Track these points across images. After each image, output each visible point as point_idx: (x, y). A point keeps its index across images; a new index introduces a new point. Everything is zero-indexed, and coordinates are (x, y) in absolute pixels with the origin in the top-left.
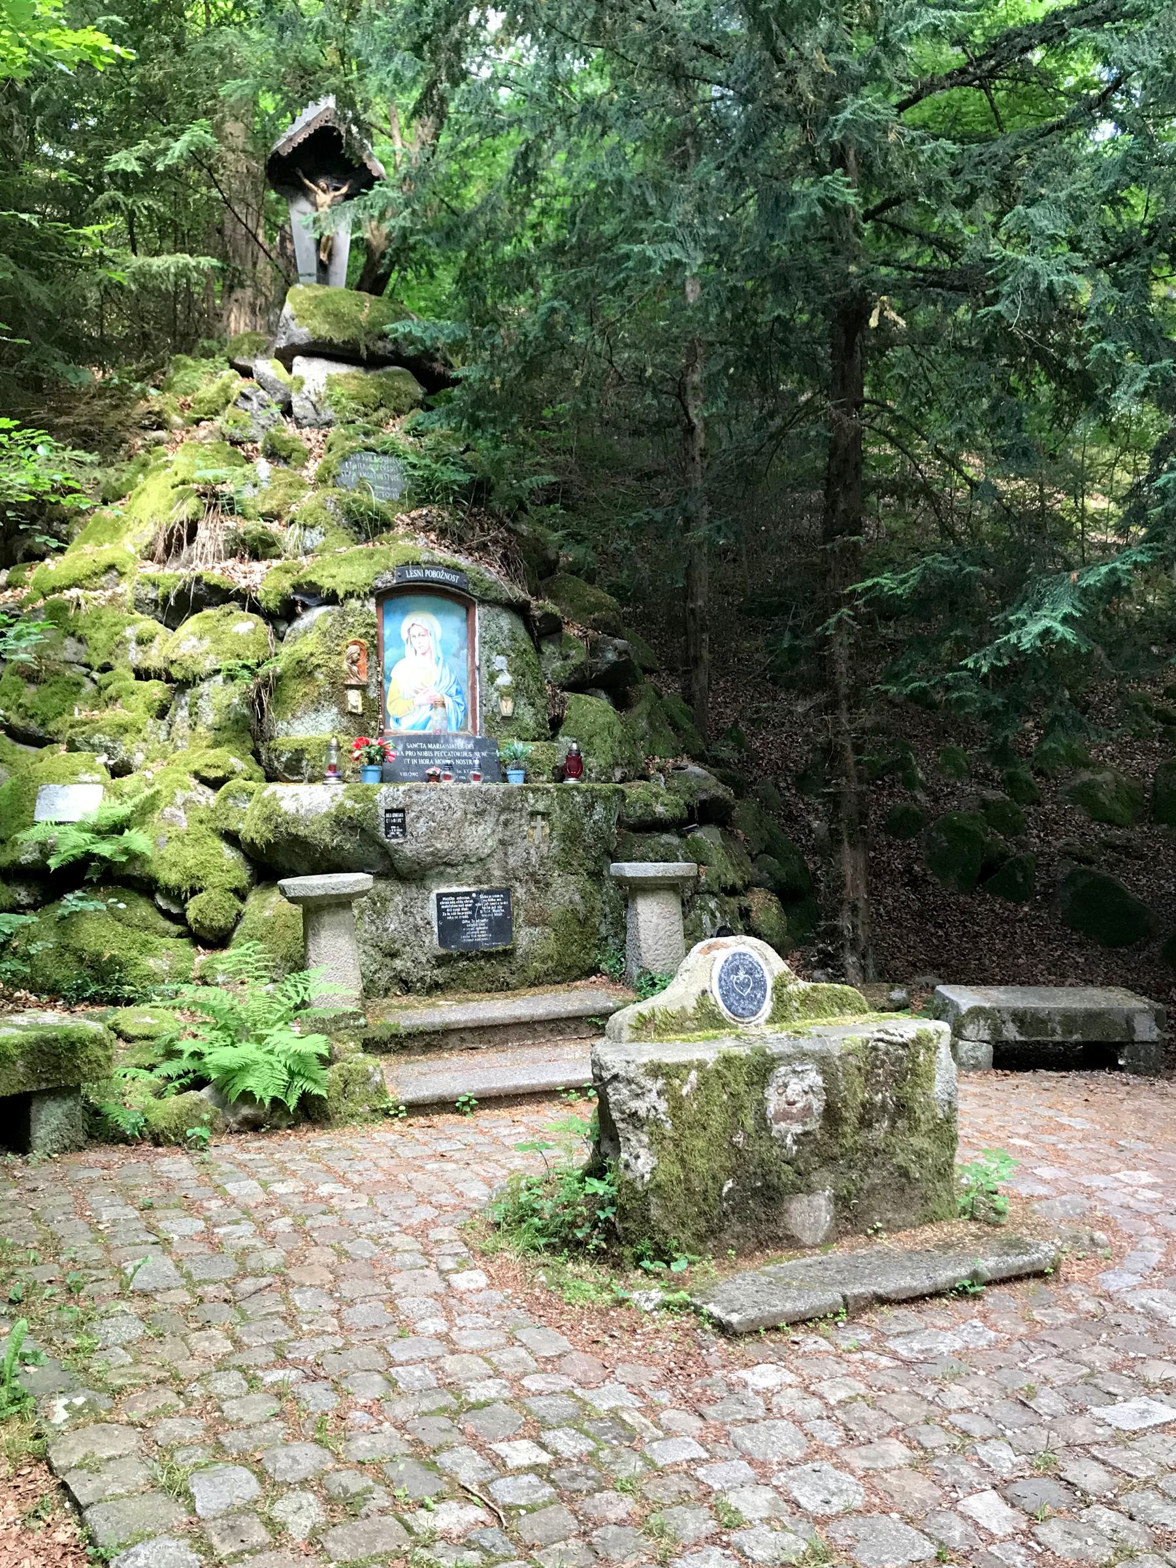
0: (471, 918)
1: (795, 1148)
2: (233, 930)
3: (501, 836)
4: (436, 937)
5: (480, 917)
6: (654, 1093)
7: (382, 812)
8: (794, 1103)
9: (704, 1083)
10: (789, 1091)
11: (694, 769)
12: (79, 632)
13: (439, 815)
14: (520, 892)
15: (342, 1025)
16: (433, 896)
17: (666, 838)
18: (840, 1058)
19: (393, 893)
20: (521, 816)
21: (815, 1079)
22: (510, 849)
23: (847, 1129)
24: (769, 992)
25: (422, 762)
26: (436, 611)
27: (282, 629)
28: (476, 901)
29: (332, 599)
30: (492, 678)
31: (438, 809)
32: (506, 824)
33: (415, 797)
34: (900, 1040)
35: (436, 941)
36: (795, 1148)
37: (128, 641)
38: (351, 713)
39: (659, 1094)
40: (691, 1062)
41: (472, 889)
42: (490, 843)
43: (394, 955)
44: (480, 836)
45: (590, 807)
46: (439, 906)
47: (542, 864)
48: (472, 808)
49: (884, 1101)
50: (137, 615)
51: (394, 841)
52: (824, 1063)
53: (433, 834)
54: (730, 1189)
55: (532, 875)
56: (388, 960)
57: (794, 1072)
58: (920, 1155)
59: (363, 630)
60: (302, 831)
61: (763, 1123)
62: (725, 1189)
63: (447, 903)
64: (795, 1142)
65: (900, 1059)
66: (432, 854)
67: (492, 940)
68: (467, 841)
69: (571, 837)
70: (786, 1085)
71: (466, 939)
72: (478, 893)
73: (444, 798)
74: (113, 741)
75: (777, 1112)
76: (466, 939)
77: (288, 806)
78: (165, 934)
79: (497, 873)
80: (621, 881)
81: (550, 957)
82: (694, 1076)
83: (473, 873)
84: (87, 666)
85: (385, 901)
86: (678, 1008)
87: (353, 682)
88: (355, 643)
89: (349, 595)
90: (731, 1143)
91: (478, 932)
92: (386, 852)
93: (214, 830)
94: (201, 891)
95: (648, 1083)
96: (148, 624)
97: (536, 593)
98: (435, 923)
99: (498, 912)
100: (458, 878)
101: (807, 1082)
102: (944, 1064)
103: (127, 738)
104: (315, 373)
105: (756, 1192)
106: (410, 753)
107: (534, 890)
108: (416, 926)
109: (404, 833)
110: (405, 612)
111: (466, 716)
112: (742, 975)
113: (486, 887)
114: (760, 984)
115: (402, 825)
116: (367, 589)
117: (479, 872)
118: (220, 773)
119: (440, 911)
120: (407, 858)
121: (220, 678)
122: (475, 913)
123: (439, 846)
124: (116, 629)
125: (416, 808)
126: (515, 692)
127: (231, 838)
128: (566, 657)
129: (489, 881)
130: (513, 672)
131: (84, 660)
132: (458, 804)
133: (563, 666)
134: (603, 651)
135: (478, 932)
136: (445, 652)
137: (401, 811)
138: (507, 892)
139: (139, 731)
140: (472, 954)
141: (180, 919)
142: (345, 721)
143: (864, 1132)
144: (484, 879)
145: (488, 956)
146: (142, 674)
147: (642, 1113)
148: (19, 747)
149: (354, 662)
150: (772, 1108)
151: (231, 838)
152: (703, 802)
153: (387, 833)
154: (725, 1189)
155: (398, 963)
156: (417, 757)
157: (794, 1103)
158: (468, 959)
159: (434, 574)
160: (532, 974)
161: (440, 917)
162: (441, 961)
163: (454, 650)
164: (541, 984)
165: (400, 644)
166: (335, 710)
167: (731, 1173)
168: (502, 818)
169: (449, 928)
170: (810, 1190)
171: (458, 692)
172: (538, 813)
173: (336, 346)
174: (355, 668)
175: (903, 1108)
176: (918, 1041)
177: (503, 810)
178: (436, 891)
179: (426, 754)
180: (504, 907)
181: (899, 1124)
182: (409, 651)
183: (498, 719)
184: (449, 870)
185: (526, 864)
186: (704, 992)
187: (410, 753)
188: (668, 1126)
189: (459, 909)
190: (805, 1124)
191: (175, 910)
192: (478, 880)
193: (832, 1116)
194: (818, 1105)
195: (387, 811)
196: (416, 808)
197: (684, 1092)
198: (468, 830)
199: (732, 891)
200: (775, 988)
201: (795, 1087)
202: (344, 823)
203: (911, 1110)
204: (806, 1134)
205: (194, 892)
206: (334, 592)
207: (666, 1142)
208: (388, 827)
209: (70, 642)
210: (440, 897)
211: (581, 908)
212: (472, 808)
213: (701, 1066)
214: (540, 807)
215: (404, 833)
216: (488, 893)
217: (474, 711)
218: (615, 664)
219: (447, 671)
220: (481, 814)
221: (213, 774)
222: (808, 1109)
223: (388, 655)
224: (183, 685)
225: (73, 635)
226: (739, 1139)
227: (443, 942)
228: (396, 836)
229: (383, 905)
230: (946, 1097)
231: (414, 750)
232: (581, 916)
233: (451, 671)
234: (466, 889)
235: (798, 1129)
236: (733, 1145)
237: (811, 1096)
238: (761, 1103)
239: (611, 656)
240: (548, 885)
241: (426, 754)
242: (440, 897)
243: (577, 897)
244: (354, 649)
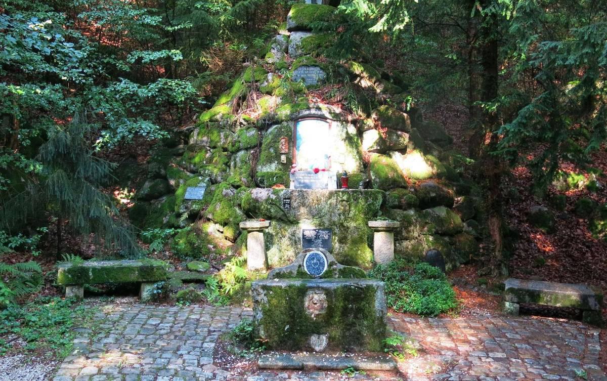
0: (315, 239)
1: (315, 319)
39: (265, 295)
62: (286, 328)
72: (319, 230)
87: (283, 152)
88: (284, 138)
108: (295, 241)
112: (315, 261)
115: (289, 204)
154: (286, 328)
170: (319, 333)
186: (300, 266)
208: (284, 204)
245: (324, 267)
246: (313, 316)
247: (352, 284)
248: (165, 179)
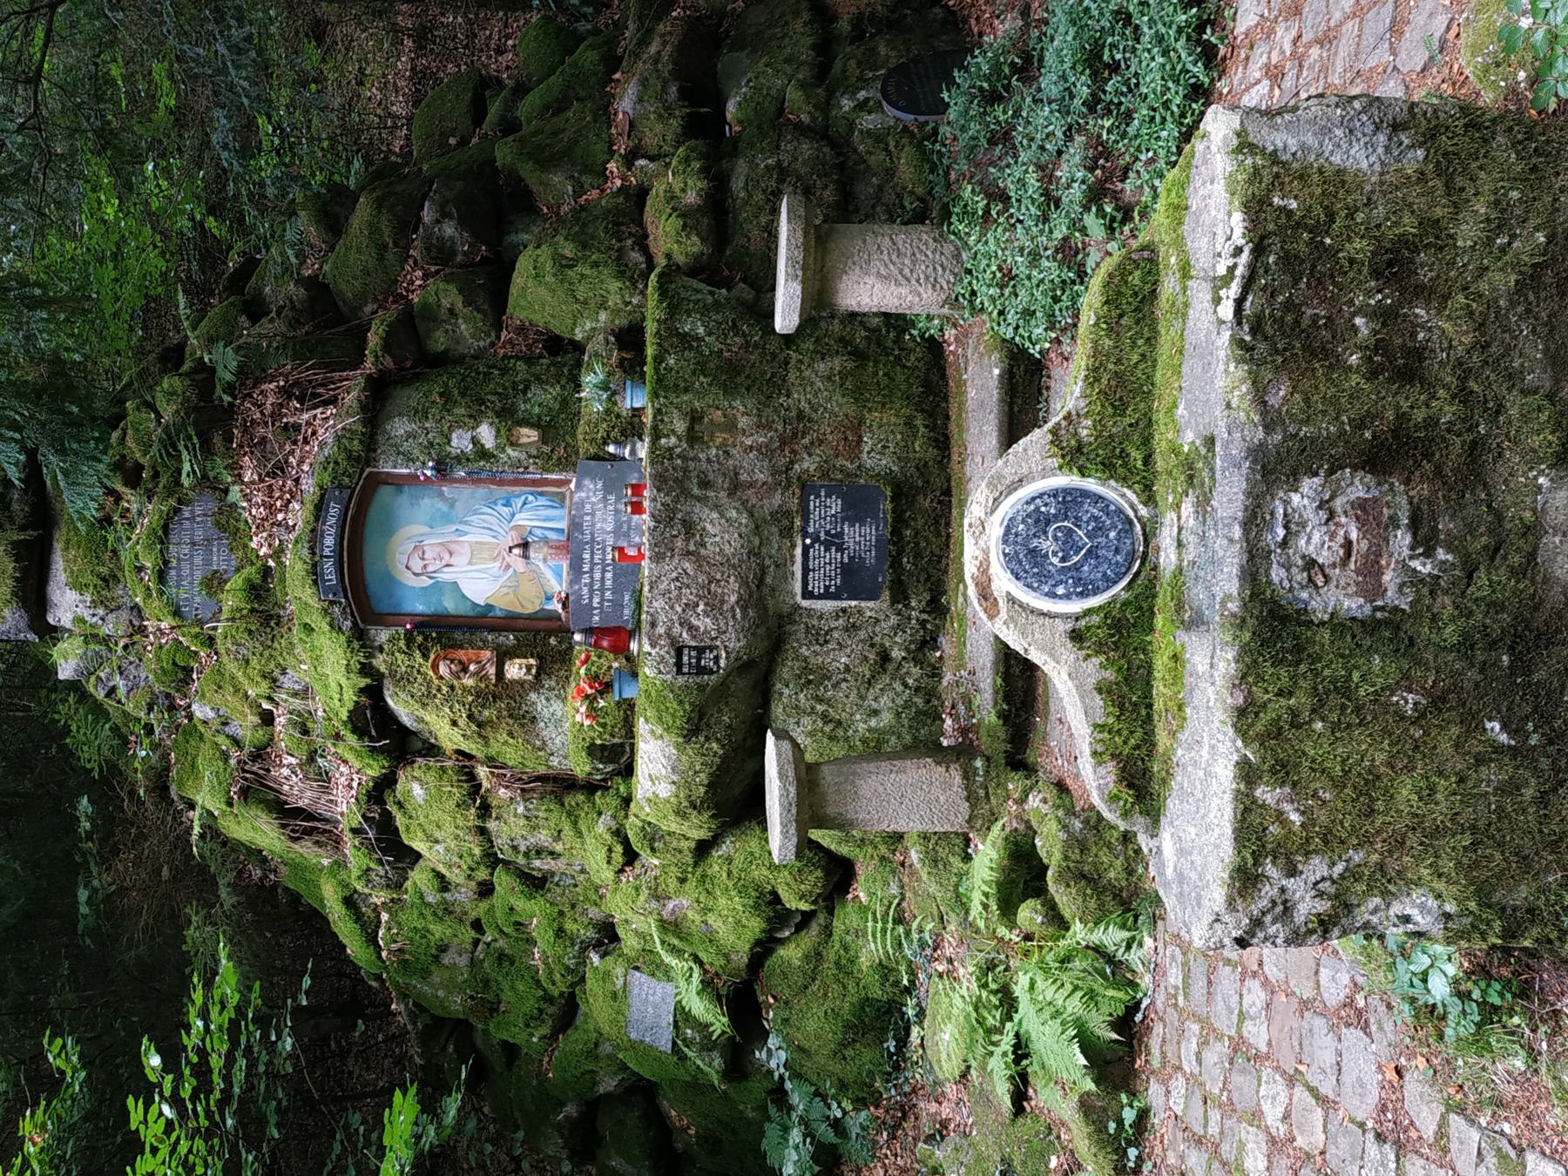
0: (840, 549)
1: (1441, 554)
2: (828, 852)
3: (723, 494)
4: (863, 604)
5: (841, 535)
6: (1290, 883)
7: (681, 680)
8: (1348, 545)
9: (1282, 771)
10: (1323, 558)
11: (625, 104)
12: (433, 951)
13: (688, 595)
14: (808, 464)
15: (982, 792)
16: (805, 603)
17: (737, 184)
18: (1268, 428)
19: (797, 658)
20: (696, 459)
21: (1303, 498)
22: (744, 477)
23: (1419, 415)
24: (1091, 484)
25: (609, 583)
26: (389, 530)
27: (419, 745)
28: (816, 539)
29: (373, 692)
30: (483, 454)
31: (679, 598)
32: (705, 484)
33: (661, 630)
34: (1245, 258)
35: (871, 604)
36: (1441, 554)
37: (445, 901)
38: (537, 676)
39: (1292, 872)
40: (1239, 796)
41: (799, 543)
42: (734, 514)
43: (885, 657)
44: (721, 531)
45: (687, 341)
46: (820, 597)
47: (769, 426)
48: (679, 543)
49: (1372, 314)
50: (408, 884)
51: (722, 663)
52: (1273, 469)
53: (715, 606)
54: (1504, 727)
55: (783, 443)
56: (891, 667)
57: (1284, 544)
58: (1501, 221)
59: (417, 654)
60: (703, 778)
61: (1386, 629)
62: (1504, 738)
63: (817, 586)
64: (1429, 553)
65: (1287, 259)
66: (744, 609)
67: (875, 518)
68: (728, 550)
69: (729, 376)
70: (1310, 564)
71: (870, 558)
73: (662, 587)
74: (573, 945)
75: (1362, 591)
76: (870, 558)
77: (665, 791)
78: (828, 931)
79: (777, 500)
80: (809, 321)
81: (909, 423)
82: (1266, 794)
83: (775, 539)
84: (476, 943)
85: (806, 669)
86: (1098, 701)
87: (492, 671)
88: (435, 667)
89: (366, 670)
90: (1415, 722)
91: (861, 538)
92: (742, 667)
93: (696, 864)
94: (774, 893)
95: (1268, 892)
96: (418, 878)
97: (357, 362)
98: (845, 604)
99: (835, 505)
100: (783, 565)
101: (1309, 514)
102: (1310, 139)
103: (569, 926)
104: (67, 604)
105: (1522, 664)
106: (596, 600)
107: (806, 441)
108: (846, 629)
109: (711, 649)
110: (390, 580)
111: (541, 494)
112: (1047, 545)
113: (798, 523)
114: (1069, 500)
115: (701, 651)
116: (356, 645)
117: (774, 529)
118: (619, 849)
119: (826, 596)
120: (749, 645)
121: (492, 825)
122: (834, 541)
123: (733, 599)
124: (427, 912)
125: (677, 629)
126: (508, 418)
127: (703, 849)
128: (451, 311)
129: (788, 514)
130: (476, 419)
131: (469, 947)
132: (671, 567)
133: (467, 320)
134: (441, 239)
135: (861, 538)
136: (447, 519)
137: (679, 652)
138: (807, 488)
139: (561, 913)
140: (894, 545)
141: (807, 917)
142: (548, 683)
143: (1432, 367)
144: (785, 522)
145: (899, 521)
146: (486, 890)
147: (1323, 906)
148: (579, 1020)
149: (465, 670)
150: (1353, 605)
151: (703, 849)
152: (684, 94)
153: (711, 672)
154: (1504, 738)
155: (896, 654)
156: (602, 590)
157: (1348, 545)
158: (900, 553)
159: (329, 541)
160: (932, 452)
161: (836, 596)
162: (900, 595)
163: (444, 508)
164: (947, 437)
165: (438, 587)
166: (533, 696)
167: (1472, 724)
168: (696, 491)
169: (853, 581)
171: (507, 504)
172: (691, 429)
173: (24, 571)
174: (472, 667)
175: (1393, 264)
176: (1255, 208)
177: (686, 493)
178: (799, 598)
179: (597, 576)
180: (828, 495)
181: (1425, 276)
182: (446, 576)
183: (547, 449)
184: (769, 580)
185: (764, 451)
186: (1076, 636)
187: (596, 600)
188: (1358, 857)
189: (827, 563)
190: (1394, 522)
191: (798, 918)
192: (787, 532)
193: (1384, 454)
194: (1358, 487)
195: (679, 672)
196: (677, 629)
197: (1295, 817)
198: (710, 551)
199: (825, 48)
200: (1083, 472)
201: (1316, 542)
202: (694, 728)
203: (1403, 241)
204: (1414, 525)
205: (776, 899)
206: (361, 690)
207: (1393, 866)
209: (447, 959)
210: (807, 594)
211: (837, 363)
212: (679, 543)
213: (1247, 774)
214: (680, 426)
215: (711, 649)
216: (806, 520)
217: (534, 483)
218: (462, 224)
219: (474, 519)
220: (689, 527)
221: (618, 857)
222: (1363, 511)
223: (450, 605)
224: (492, 860)
225: (436, 957)
226: (1409, 701)
227: (873, 596)
228: (717, 659)
229: (812, 672)
230: (1382, 138)
231: (591, 591)
232: (850, 365)
233: (476, 512)
234: (798, 551)
235: (1402, 540)
236: (1421, 715)
237: (1338, 503)
238: (1339, 625)
239: (449, 230)
240: (801, 416)
241: (597, 576)
242: (807, 594)
243: (821, 367)
244: (443, 669)
245: (1085, 494)
246: (1423, 567)
247: (1227, 310)
248: (593, 1106)
